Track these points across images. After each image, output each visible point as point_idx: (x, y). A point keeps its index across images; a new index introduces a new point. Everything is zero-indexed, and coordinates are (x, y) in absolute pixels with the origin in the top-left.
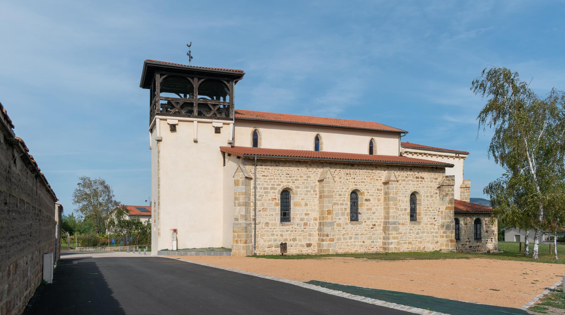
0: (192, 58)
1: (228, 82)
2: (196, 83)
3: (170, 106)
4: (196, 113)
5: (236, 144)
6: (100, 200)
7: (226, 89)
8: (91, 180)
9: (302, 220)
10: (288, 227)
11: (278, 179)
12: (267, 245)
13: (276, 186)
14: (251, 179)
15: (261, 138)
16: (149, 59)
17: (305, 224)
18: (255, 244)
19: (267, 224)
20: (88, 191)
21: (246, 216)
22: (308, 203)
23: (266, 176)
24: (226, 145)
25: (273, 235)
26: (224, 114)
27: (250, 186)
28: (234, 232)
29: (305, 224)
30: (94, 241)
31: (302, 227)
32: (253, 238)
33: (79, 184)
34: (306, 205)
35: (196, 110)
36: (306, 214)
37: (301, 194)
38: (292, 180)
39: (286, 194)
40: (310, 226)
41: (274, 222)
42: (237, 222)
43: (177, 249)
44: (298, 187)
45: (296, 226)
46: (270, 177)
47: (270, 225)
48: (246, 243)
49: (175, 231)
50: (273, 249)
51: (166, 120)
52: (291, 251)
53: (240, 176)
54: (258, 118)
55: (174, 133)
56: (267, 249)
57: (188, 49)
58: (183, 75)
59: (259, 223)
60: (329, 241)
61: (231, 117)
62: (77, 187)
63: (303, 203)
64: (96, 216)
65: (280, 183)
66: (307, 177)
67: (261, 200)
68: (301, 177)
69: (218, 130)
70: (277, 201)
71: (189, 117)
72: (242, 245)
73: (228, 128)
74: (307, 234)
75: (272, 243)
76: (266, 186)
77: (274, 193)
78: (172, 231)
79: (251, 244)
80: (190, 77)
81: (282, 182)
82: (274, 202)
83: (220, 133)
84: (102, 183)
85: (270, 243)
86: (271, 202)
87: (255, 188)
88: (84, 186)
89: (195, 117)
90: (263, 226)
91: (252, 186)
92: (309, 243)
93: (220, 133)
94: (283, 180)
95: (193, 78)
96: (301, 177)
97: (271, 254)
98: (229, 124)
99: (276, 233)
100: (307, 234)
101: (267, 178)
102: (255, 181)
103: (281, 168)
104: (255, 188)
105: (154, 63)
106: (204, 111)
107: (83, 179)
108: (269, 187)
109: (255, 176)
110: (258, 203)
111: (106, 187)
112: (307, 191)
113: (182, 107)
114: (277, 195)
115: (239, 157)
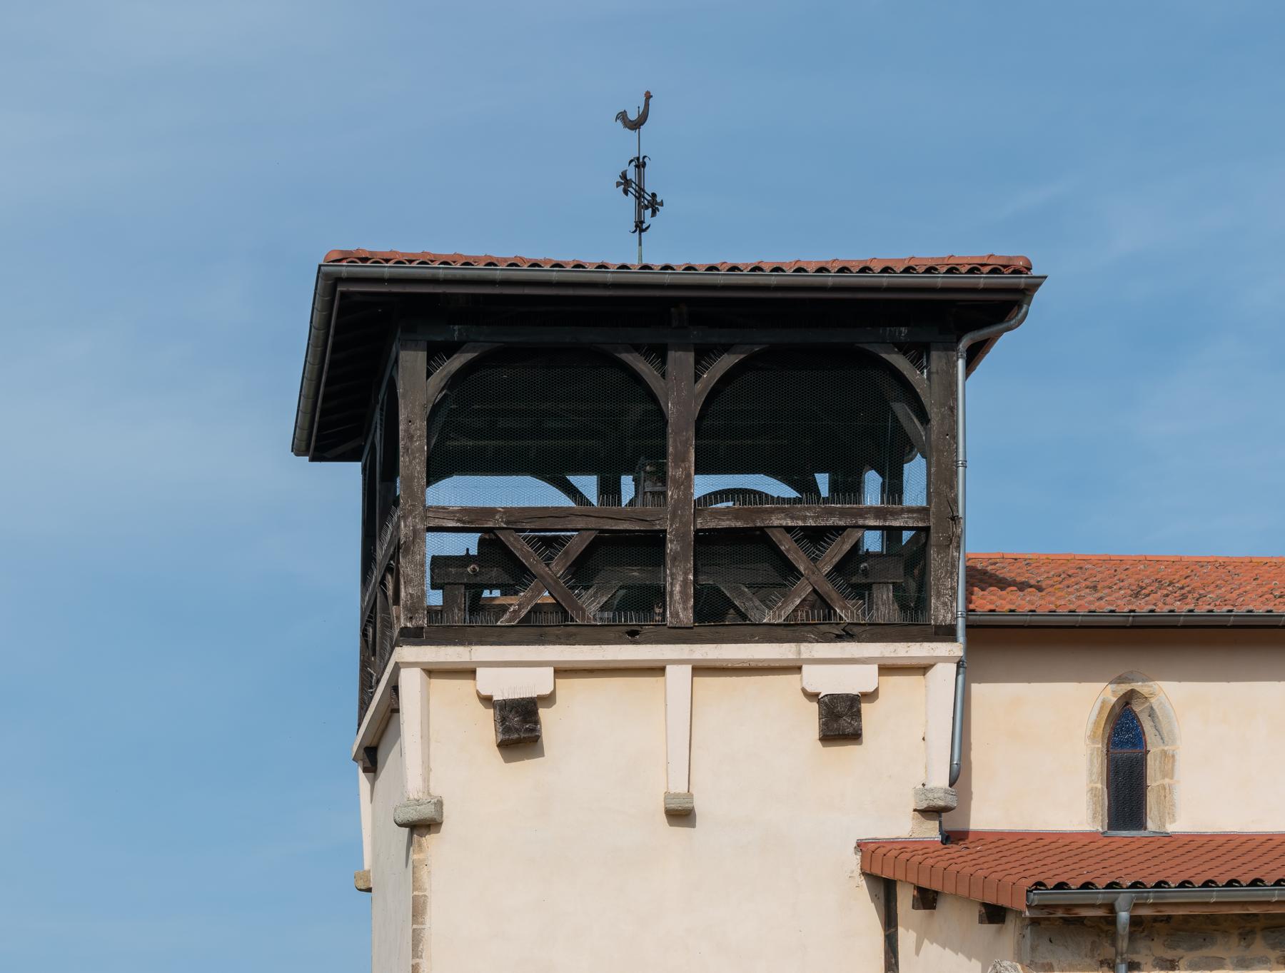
1: (918, 352)
2: (681, 386)
3: (494, 574)
4: (680, 609)
7: (902, 410)
15: (1169, 758)
16: (351, 246)
24: (901, 825)
35: (679, 584)
51: (468, 672)
54: (1142, 606)
55: (526, 768)
57: (627, 144)
69: (840, 720)
71: (633, 636)
73: (917, 702)
80: (636, 348)
83: (854, 736)
89: (680, 635)
93: (854, 736)
95: (659, 354)
98: (922, 669)
105: (387, 270)
106: (738, 588)
113: (582, 571)
115: (994, 914)
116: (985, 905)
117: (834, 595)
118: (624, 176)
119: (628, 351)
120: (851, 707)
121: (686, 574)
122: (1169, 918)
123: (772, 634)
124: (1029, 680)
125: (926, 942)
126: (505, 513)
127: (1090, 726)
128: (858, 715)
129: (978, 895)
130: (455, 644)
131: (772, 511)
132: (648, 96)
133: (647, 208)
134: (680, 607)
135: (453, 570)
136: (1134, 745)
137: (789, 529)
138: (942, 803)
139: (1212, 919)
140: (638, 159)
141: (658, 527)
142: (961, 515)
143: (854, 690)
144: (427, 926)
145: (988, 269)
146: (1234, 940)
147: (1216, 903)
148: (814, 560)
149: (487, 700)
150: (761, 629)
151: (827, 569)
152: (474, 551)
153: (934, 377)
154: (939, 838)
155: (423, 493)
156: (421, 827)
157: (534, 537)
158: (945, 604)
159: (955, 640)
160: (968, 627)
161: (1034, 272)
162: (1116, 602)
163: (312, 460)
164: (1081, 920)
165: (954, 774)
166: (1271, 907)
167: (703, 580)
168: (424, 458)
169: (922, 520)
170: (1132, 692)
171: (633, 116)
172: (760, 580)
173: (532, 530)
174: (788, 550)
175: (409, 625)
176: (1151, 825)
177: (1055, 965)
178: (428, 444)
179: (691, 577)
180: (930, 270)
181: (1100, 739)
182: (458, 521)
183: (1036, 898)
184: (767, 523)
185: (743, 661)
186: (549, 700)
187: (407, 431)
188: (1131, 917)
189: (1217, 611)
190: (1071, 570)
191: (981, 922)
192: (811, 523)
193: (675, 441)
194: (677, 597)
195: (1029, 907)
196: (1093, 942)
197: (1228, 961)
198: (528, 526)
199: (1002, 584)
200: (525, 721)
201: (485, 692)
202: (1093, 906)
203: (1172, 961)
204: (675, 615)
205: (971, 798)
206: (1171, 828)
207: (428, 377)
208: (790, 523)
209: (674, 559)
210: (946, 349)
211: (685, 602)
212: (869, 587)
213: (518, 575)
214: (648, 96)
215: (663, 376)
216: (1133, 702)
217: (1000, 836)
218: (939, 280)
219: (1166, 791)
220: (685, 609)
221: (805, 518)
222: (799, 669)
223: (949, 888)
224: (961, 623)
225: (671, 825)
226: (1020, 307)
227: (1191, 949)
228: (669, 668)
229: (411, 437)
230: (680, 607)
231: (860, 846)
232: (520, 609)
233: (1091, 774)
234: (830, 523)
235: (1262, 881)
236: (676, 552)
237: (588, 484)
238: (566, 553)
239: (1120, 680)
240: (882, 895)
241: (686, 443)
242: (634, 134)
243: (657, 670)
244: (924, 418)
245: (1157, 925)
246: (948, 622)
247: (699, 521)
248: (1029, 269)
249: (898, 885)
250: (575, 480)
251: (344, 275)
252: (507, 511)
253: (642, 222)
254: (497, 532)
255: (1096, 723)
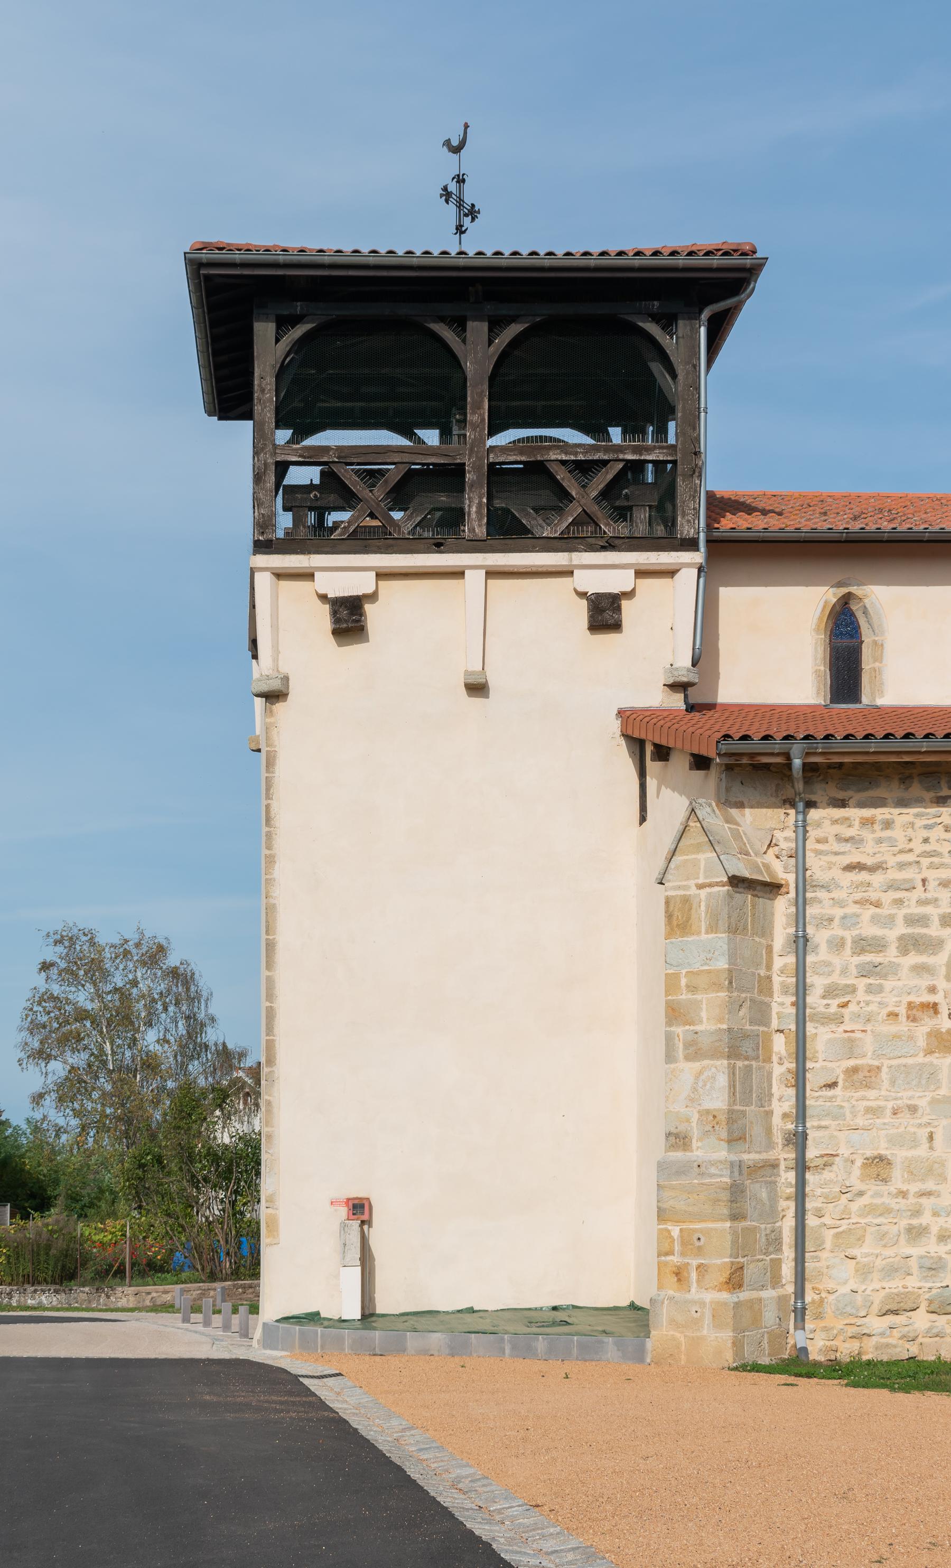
0: (473, 213)
1: (668, 322)
2: (478, 351)
3: (332, 498)
4: (476, 525)
5: (733, 688)
6: (150, 1038)
7: (656, 368)
8: (101, 939)
12: (878, 1299)
13: (934, 930)
14: (773, 888)
15: (879, 646)
16: (213, 239)
18: (800, 1293)
19: (878, 1166)
20: (83, 998)
21: (732, 1117)
23: (872, 869)
24: (655, 697)
25: (916, 1233)
26: (642, 516)
27: (765, 930)
28: (662, 1215)
30: (66, 1254)
32: (788, 1253)
33: (46, 967)
35: (474, 504)
41: (922, 1151)
42: (678, 1155)
43: (368, 1316)
47: (897, 1173)
48: (735, 1280)
49: (359, 1209)
50: (921, 1321)
51: (308, 576)
53: (703, 873)
54: (856, 526)
55: (355, 651)
56: (877, 1324)
57: (449, 165)
58: (404, 310)
59: (828, 1160)
61: (685, 529)
62: (40, 981)
64: (129, 1122)
67: (839, 1020)
69: (605, 614)
71: (439, 547)
72: (710, 1296)
73: (665, 599)
75: (913, 1282)
76: (870, 931)
77: (920, 969)
78: (343, 1211)
79: (769, 1294)
80: (442, 319)
82: (922, 1031)
83: (616, 626)
84: (155, 956)
85: (895, 1285)
86: (903, 1026)
87: (801, 943)
88: (70, 975)
89: (476, 546)
90: (855, 1180)
91: (782, 931)
93: (616, 626)
95: (459, 324)
97: (903, 1351)
98: (670, 573)
101: (877, 879)
102: (801, 903)
104: (801, 943)
105: (237, 257)
106: (521, 511)
107: (65, 940)
108: (892, 935)
109: (802, 870)
110: (821, 1038)
111: (181, 977)
113: (401, 494)
115: (700, 762)
116: (693, 755)
117: (599, 514)
118: (445, 189)
119: (434, 322)
120: (613, 603)
121: (481, 498)
122: (840, 765)
123: (549, 545)
124: (766, 585)
125: (663, 787)
126: (337, 450)
127: (815, 621)
128: (618, 609)
129: (687, 748)
130: (297, 553)
131: (549, 448)
132: (466, 126)
133: (466, 215)
134: (476, 524)
135: (299, 496)
136: (852, 637)
137: (563, 463)
138: (685, 679)
139: (877, 766)
140: (458, 176)
141: (458, 461)
142: (702, 450)
143: (615, 590)
144: (277, 774)
145: (721, 253)
146: (895, 784)
147: (874, 753)
148: (584, 487)
149: (323, 598)
150: (541, 541)
151: (594, 494)
152: (317, 481)
153: (681, 340)
154: (684, 707)
155: (273, 434)
156: (273, 697)
157: (360, 470)
158: (689, 521)
159: (698, 550)
160: (708, 541)
161: (758, 255)
162: (840, 523)
163: (220, 419)
164: (767, 766)
165: (696, 657)
166: (921, 756)
167: (498, 503)
168: (273, 407)
169: (671, 455)
170: (849, 593)
171: (455, 143)
172: (543, 503)
173: (359, 464)
174: (563, 479)
175: (261, 538)
176: (865, 700)
177: (746, 803)
178: (277, 396)
179: (485, 500)
180: (673, 253)
181: (823, 632)
182: (300, 456)
183: (723, 748)
184: (546, 457)
185: (526, 567)
186: (373, 597)
187: (260, 385)
188: (804, 764)
189: (915, 529)
190: (819, 503)
191: (691, 769)
193: (472, 392)
194: (474, 516)
195: (719, 754)
196: (778, 785)
197: (890, 801)
198: (355, 460)
199: (749, 509)
200: (352, 614)
201: (321, 592)
202: (772, 754)
203: (843, 800)
204: (472, 530)
205: (718, 678)
206: (880, 702)
207: (276, 343)
208: (564, 457)
209: (472, 486)
210: (690, 319)
211: (480, 520)
212: (630, 508)
213: (348, 499)
214: (466, 126)
215: (464, 341)
216: (851, 602)
217: (741, 707)
218: (681, 261)
219: (876, 672)
220: (480, 526)
221: (576, 454)
222: (572, 573)
223: (679, 745)
224: (702, 536)
225: (469, 696)
226: (749, 284)
227: (859, 791)
229: (263, 391)
230: (476, 524)
231: (620, 713)
232: (349, 526)
233: (816, 659)
234: (596, 457)
235: (913, 735)
236: (473, 481)
237: (431, 437)
238: (386, 481)
239: (839, 585)
240: (638, 752)
241: (481, 395)
242: (456, 156)
243: (458, 574)
244: (674, 376)
245: (831, 771)
246: (691, 536)
247: (491, 456)
248: (754, 252)
249: (646, 744)
250: (420, 433)
251: (204, 261)
253: (462, 226)
254: (331, 465)
255: (820, 619)
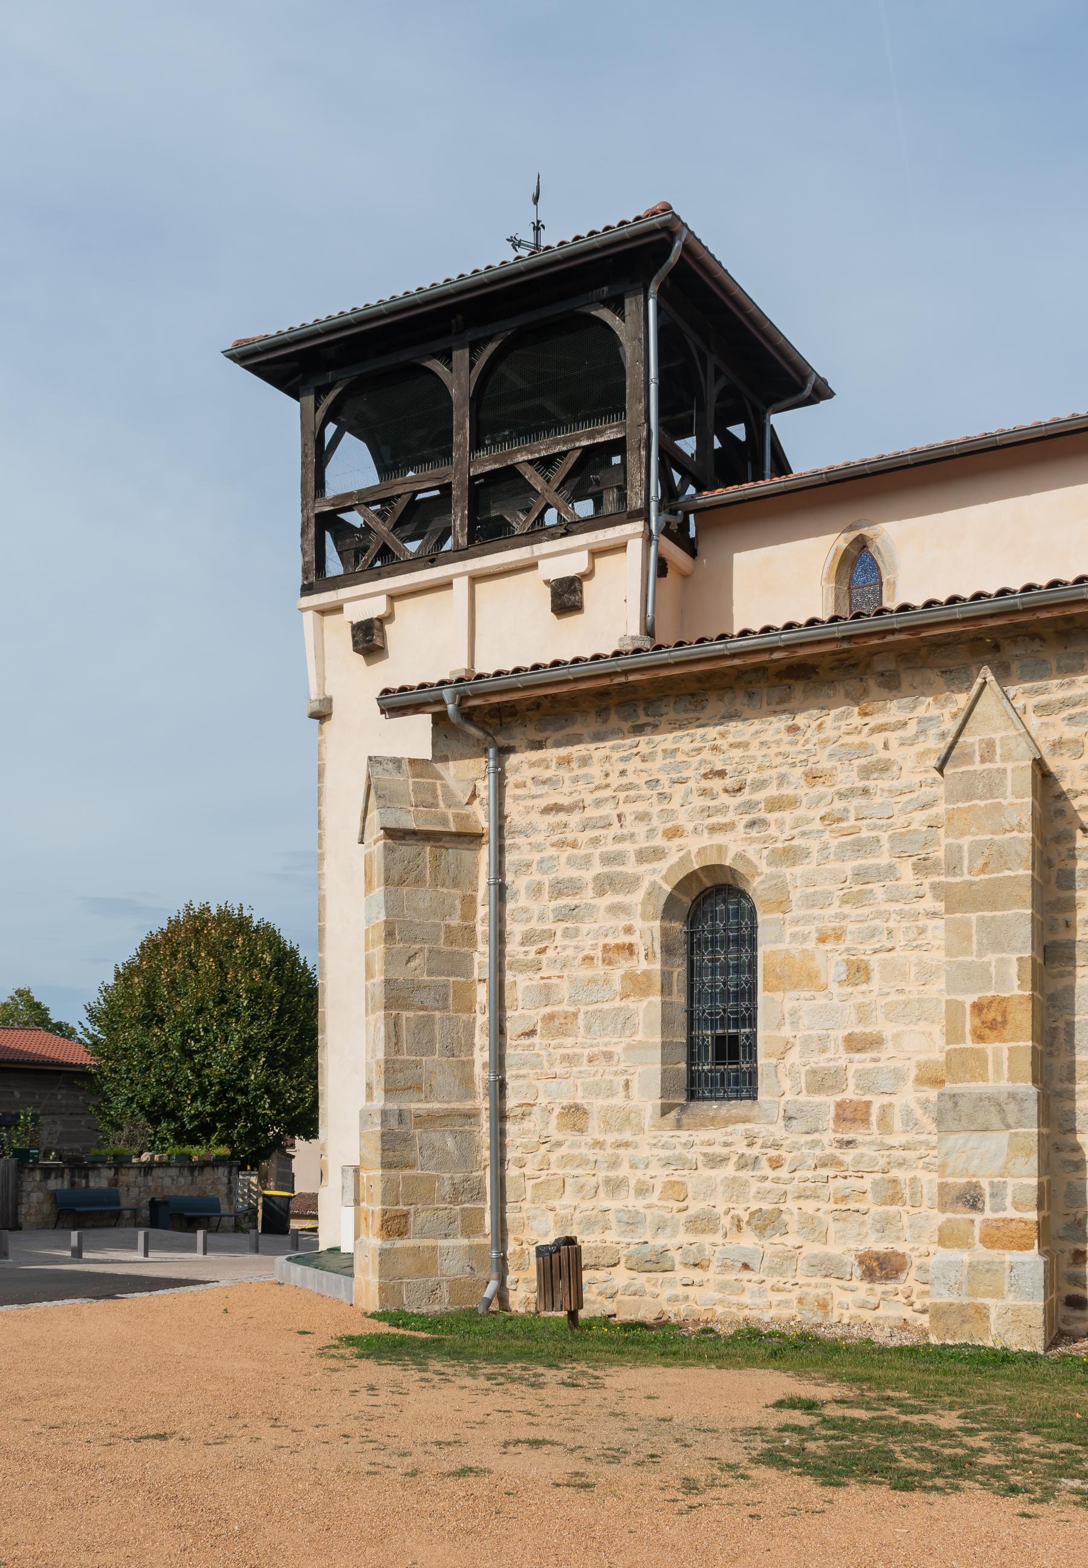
9: (822, 1081)
10: (716, 1135)
11: (642, 817)
13: (630, 868)
17: (852, 1115)
22: (875, 961)
23: (569, 809)
25: (615, 1186)
29: (852, 1115)
31: (828, 1137)
34: (858, 972)
36: (856, 1044)
37: (811, 901)
38: (750, 806)
39: (712, 916)
40: (885, 1125)
41: (619, 1100)
44: (790, 855)
45: (778, 1131)
46: (591, 813)
52: (606, 1293)
60: (989, 1241)
63: (831, 963)
65: (659, 841)
66: (866, 772)
68: (813, 777)
70: (643, 965)
74: (866, 1183)
76: (567, 873)
77: (615, 910)
80: (434, 356)
81: (674, 833)
89: (460, 554)
92: (881, 1247)
94: (682, 820)
96: (813, 777)
99: (634, 1177)
100: (866, 1183)
103: (665, 740)
109: (501, 817)
110: (518, 984)
112: (862, 876)
114: (638, 924)
119: (429, 360)
121: (463, 511)
137: (531, 462)
182: (332, 505)
184: (516, 460)
185: (498, 566)
192: (544, 453)
194: (458, 528)
197: (586, 736)
203: (540, 742)
208: (530, 457)
221: (539, 452)
228: (454, 581)
234: (556, 451)
239: (851, 528)
252: (360, 492)
